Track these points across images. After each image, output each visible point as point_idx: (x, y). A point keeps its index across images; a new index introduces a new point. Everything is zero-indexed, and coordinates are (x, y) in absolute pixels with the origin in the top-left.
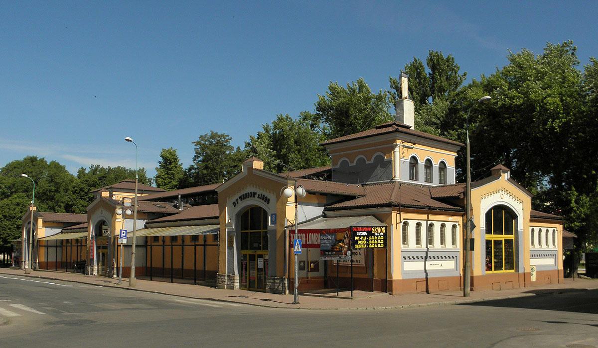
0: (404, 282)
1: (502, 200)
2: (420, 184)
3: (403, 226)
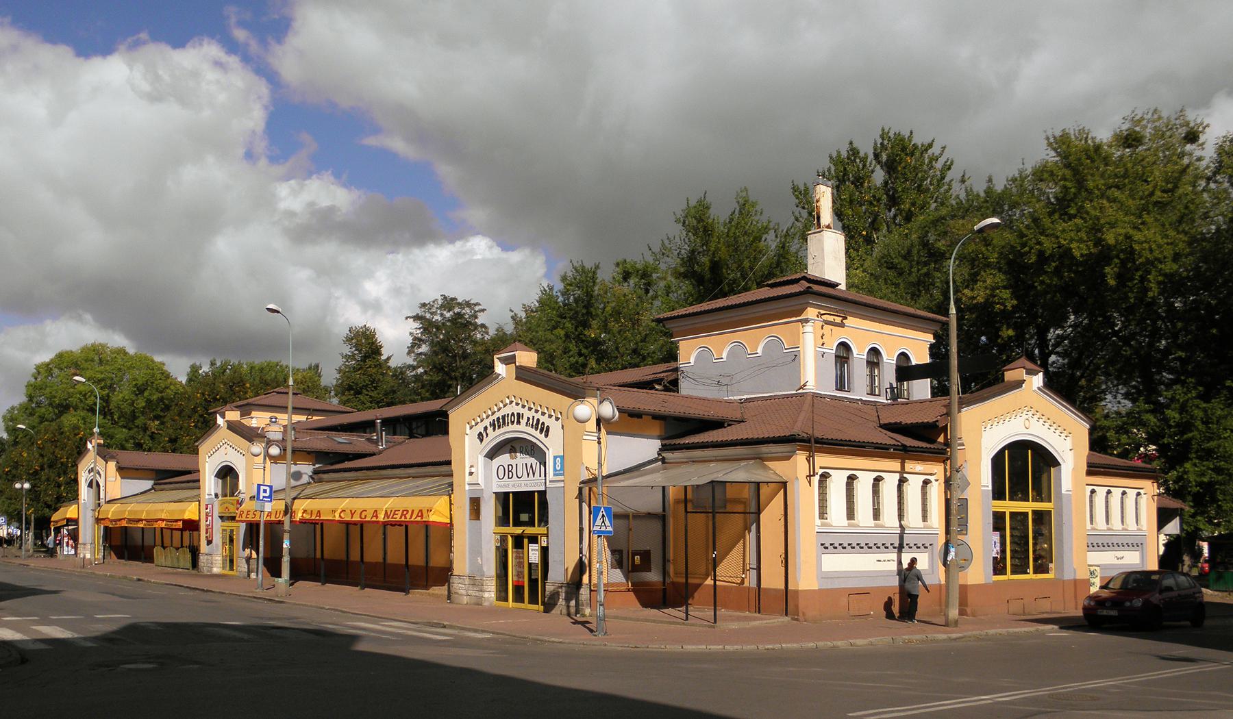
0: (823, 595)
1: (1026, 431)
2: (858, 398)
3: (820, 482)
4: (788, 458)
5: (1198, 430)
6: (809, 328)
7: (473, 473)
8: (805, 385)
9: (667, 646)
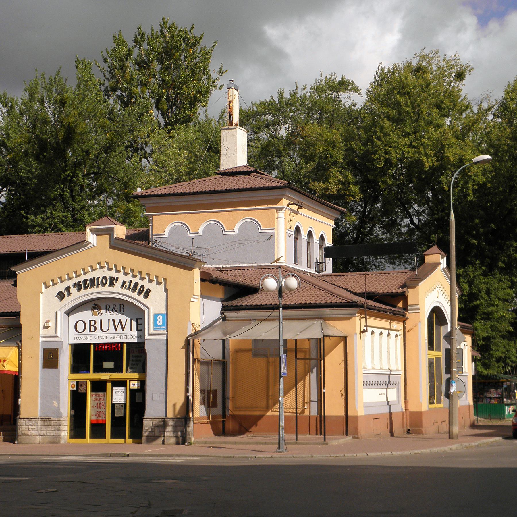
4: (349, 318)
5: (483, 298)
6: (282, 214)
7: (49, 327)
8: (279, 259)
9: (357, 454)
